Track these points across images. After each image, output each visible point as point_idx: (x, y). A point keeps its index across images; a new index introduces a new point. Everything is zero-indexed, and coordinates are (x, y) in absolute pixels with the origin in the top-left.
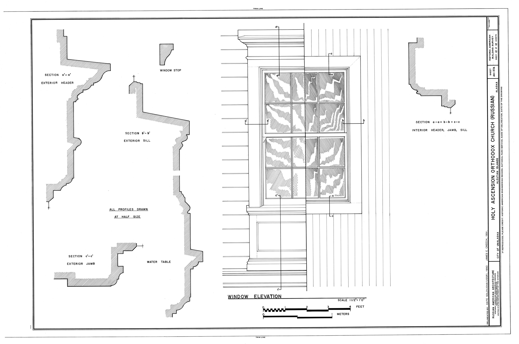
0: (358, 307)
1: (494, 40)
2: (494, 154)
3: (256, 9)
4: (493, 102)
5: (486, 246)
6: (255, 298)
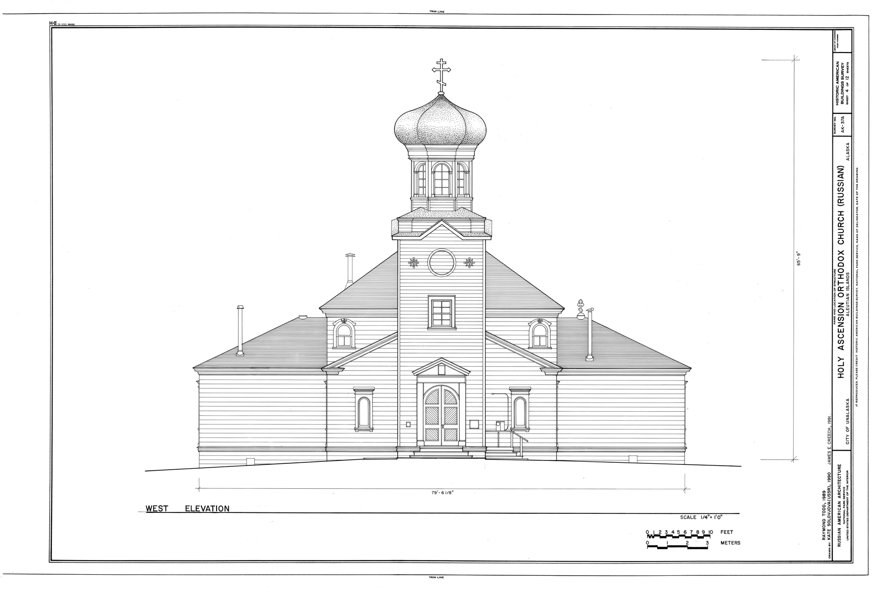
1: (845, 68)
2: (843, 266)
5: (829, 440)
6: (187, 512)
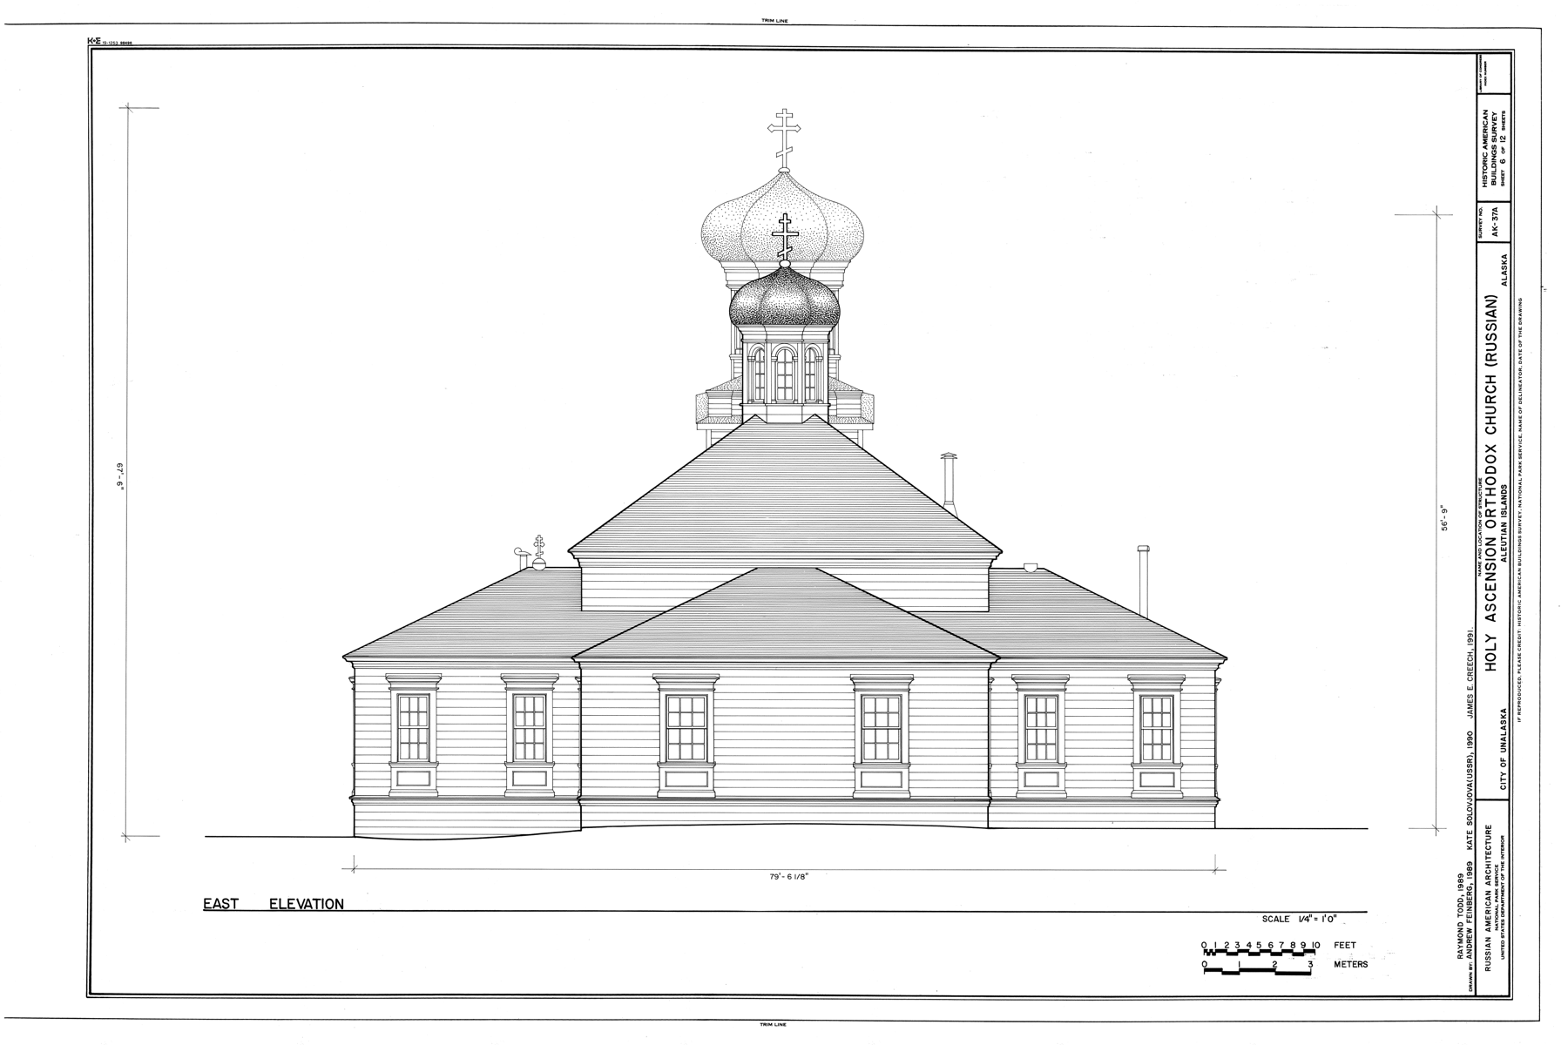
1: (1499, 122)
2: (1495, 473)
3: (768, 22)
4: (1492, 314)
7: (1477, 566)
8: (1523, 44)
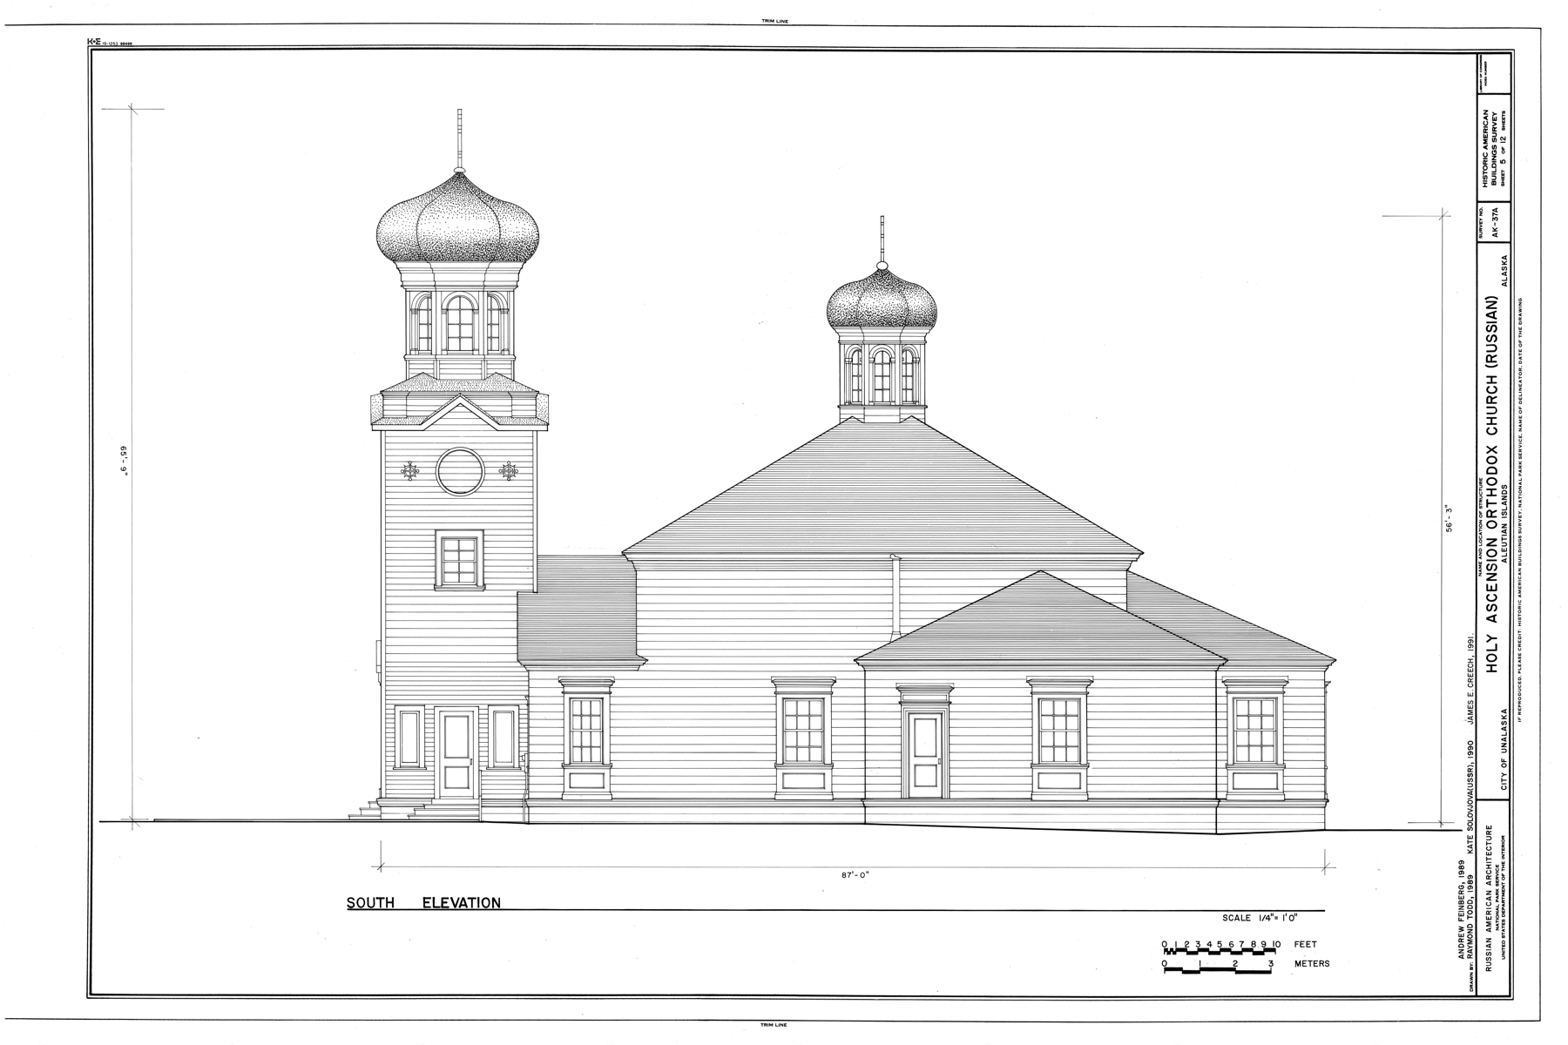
0: (1298, 946)
1: (1499, 122)
2: (1496, 473)
3: (768, 22)
4: (1492, 315)
5: (1470, 681)
6: (426, 908)
7: (1478, 565)
8: (1523, 44)
